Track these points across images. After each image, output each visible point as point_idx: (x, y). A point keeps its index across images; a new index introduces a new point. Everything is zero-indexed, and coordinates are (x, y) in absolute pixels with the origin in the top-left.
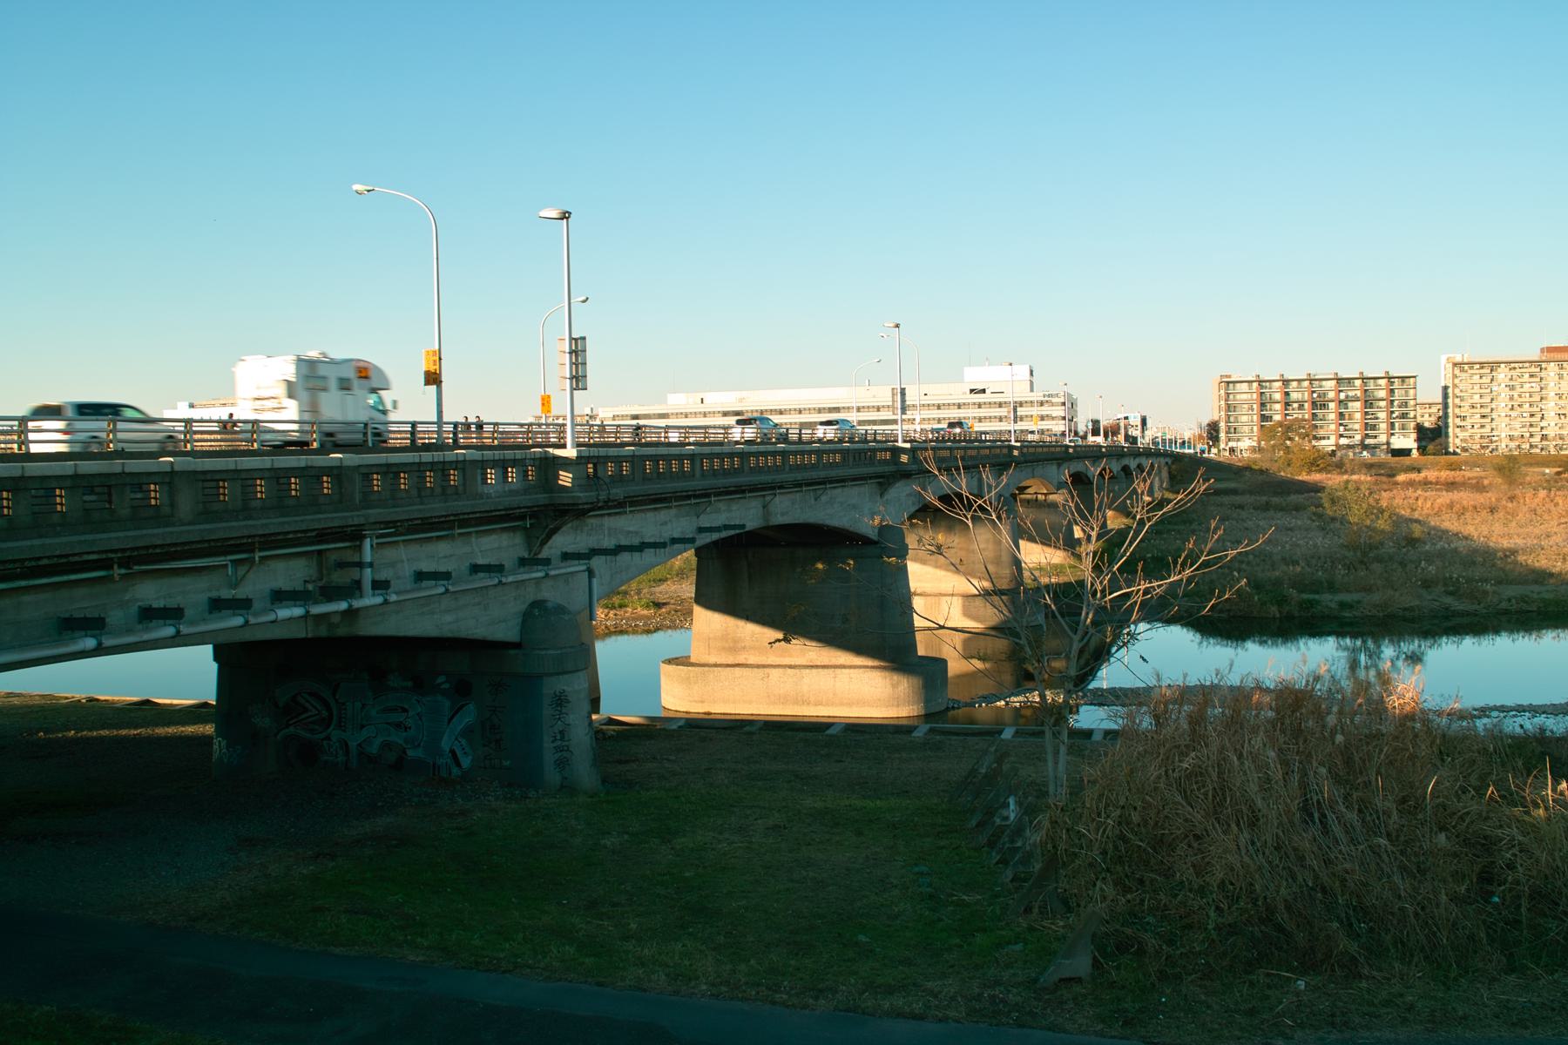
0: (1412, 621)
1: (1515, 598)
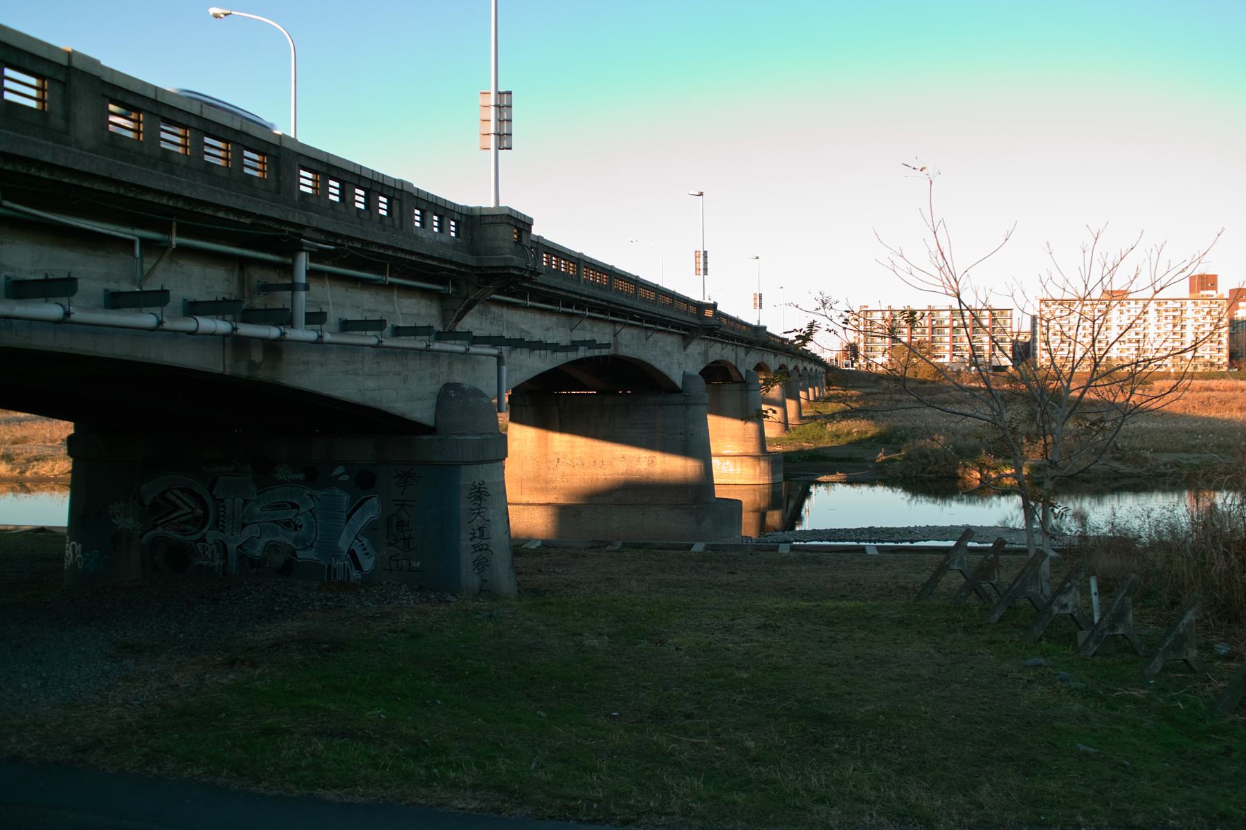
0: (1088, 481)
1: (1170, 463)
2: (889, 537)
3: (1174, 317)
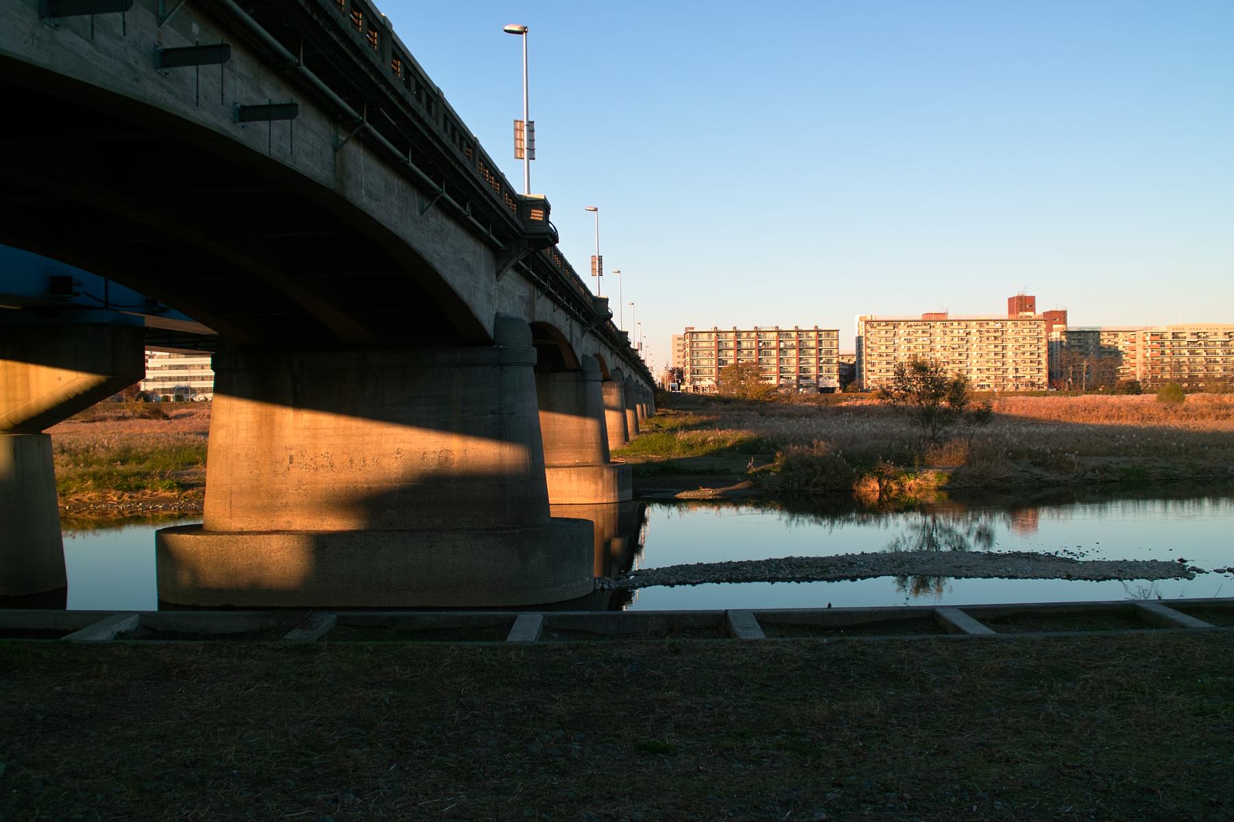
2: (821, 573)
3: (996, 338)
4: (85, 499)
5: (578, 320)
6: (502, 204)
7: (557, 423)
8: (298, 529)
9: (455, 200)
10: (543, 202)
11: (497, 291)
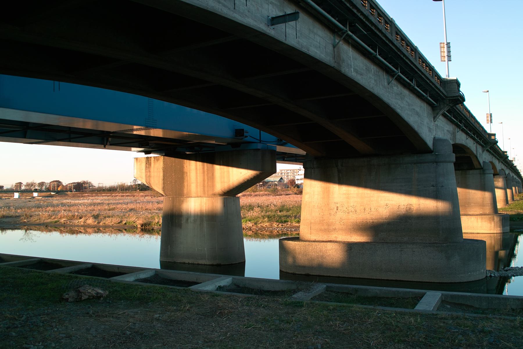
4: (264, 226)
5: (480, 145)
6: (433, 81)
7: (471, 194)
8: (340, 240)
9: (407, 78)
10: (456, 81)
11: (434, 127)
